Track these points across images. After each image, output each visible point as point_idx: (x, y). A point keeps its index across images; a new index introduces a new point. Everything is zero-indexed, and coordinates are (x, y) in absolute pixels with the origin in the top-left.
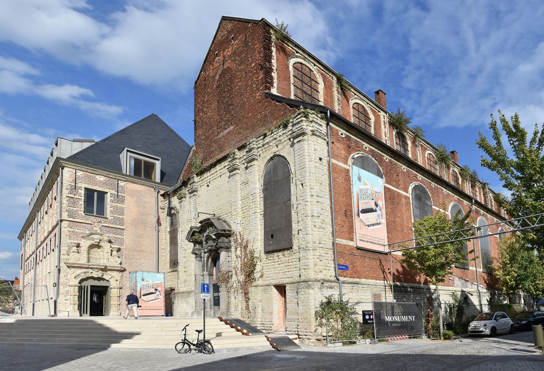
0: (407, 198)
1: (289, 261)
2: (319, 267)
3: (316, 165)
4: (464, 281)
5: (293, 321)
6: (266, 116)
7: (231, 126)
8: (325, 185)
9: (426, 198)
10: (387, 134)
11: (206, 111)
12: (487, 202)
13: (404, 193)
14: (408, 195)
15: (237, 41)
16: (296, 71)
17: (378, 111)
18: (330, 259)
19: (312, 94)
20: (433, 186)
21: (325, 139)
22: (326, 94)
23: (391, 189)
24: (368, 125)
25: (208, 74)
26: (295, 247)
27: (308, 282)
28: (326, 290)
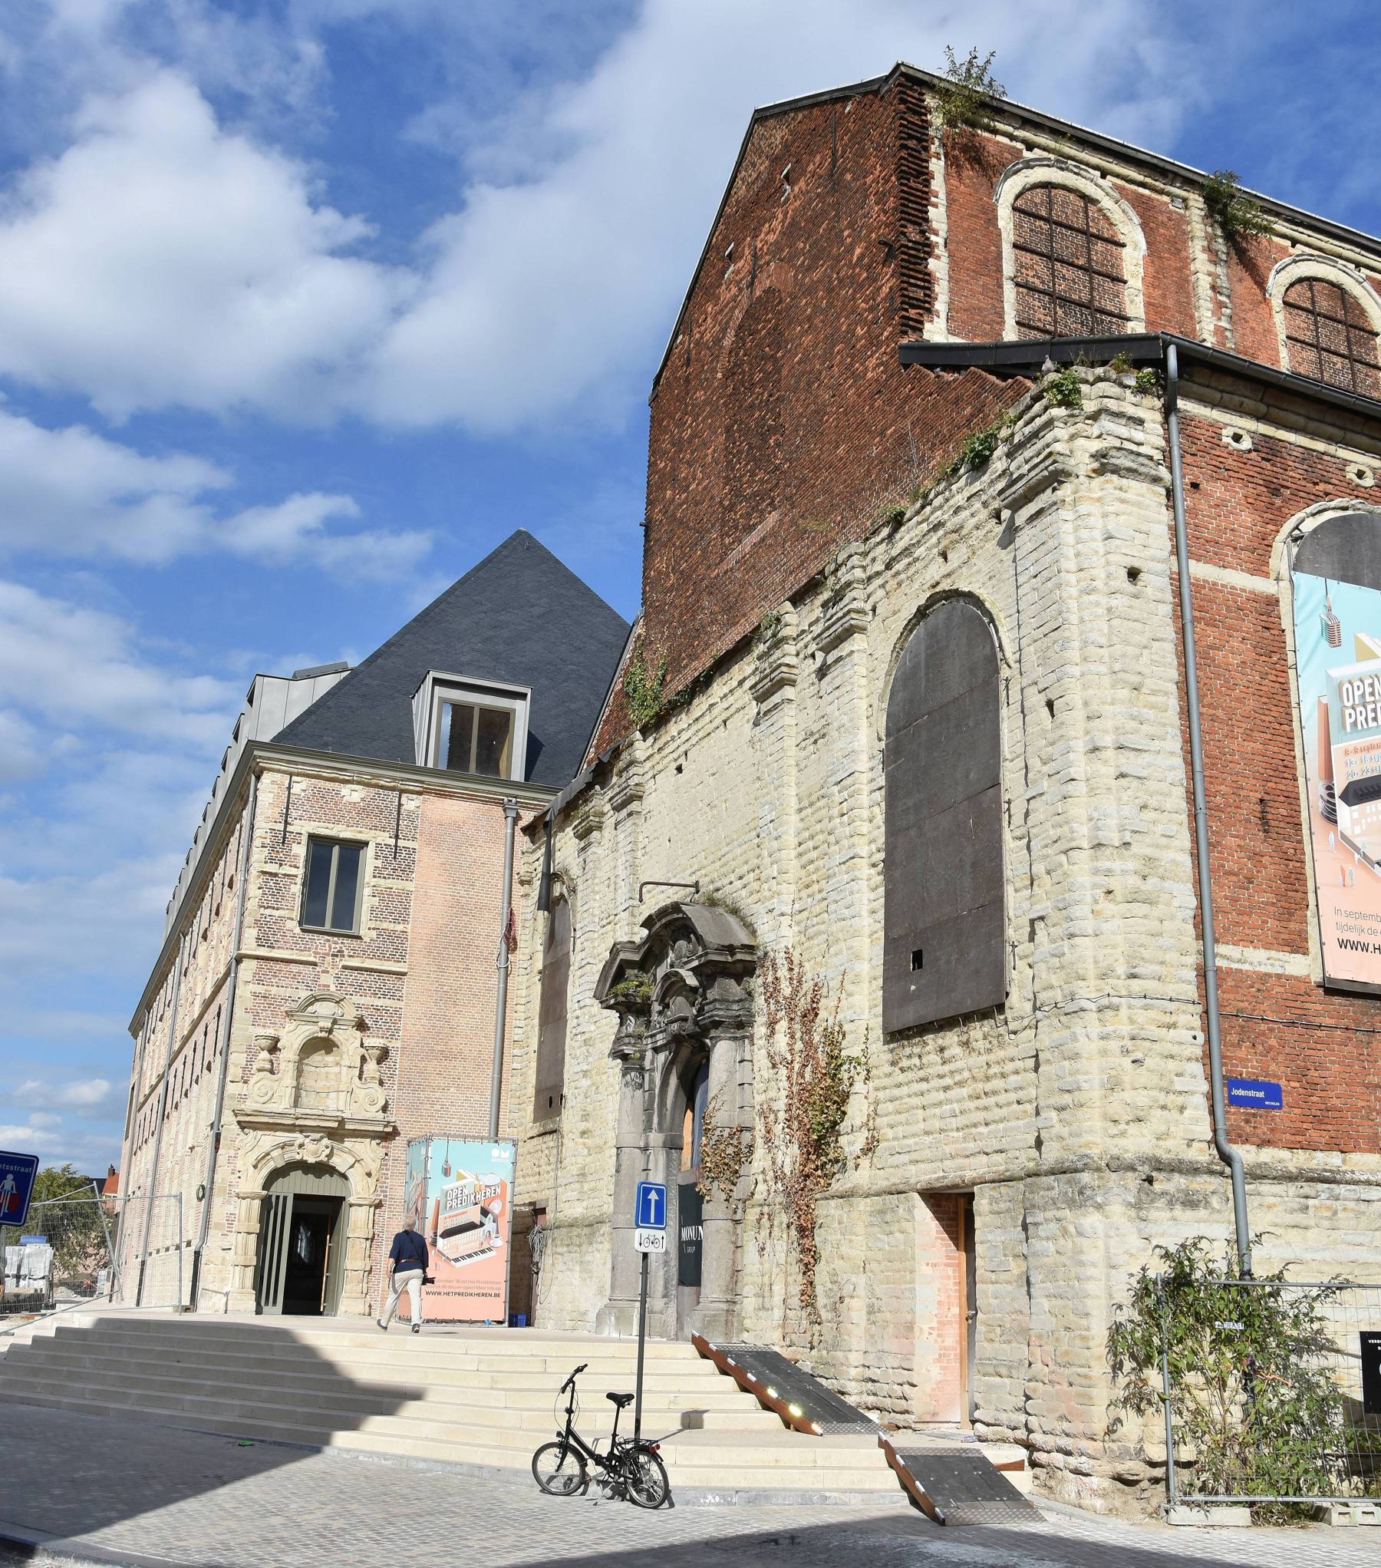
1: (991, 1072)
3: (1114, 603)
5: (1003, 1371)
6: (901, 440)
7: (770, 513)
8: (1154, 693)
11: (685, 479)
19: (1091, 301)
21: (1156, 480)
26: (1017, 1002)
27: (1076, 1171)
28: (1168, 1214)
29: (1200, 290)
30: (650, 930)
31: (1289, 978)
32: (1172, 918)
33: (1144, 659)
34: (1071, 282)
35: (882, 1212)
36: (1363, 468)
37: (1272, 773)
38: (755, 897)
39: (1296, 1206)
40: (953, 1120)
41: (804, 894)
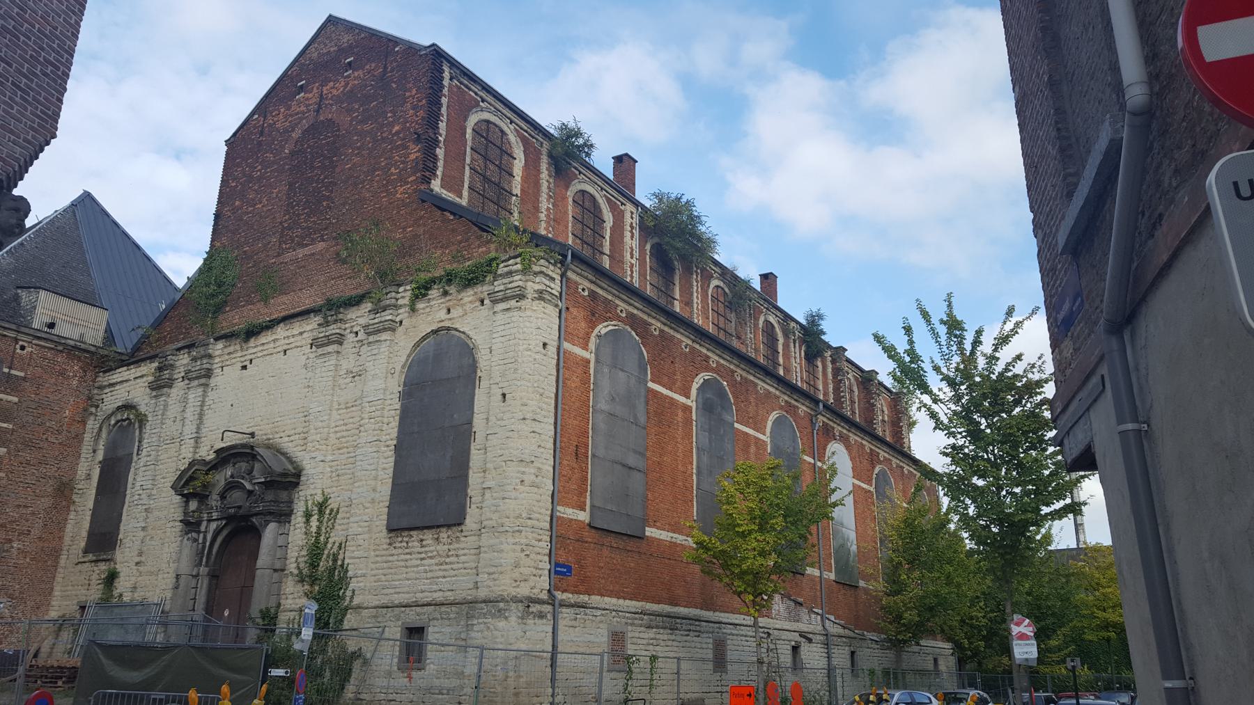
0: (687, 409)
1: (450, 553)
2: (522, 570)
3: (537, 357)
4: (792, 604)
5: (445, 692)
7: (319, 242)
8: (547, 397)
9: (723, 408)
12: (842, 394)
13: (682, 399)
14: (688, 402)
15: (360, 72)
18: (544, 552)
19: (500, 183)
20: (739, 379)
21: (557, 306)
22: (525, 179)
25: (271, 121)
26: (470, 522)
27: (497, 602)
28: (533, 622)
30: (1040, 660)
32: (545, 494)
33: (545, 383)
35: (375, 617)
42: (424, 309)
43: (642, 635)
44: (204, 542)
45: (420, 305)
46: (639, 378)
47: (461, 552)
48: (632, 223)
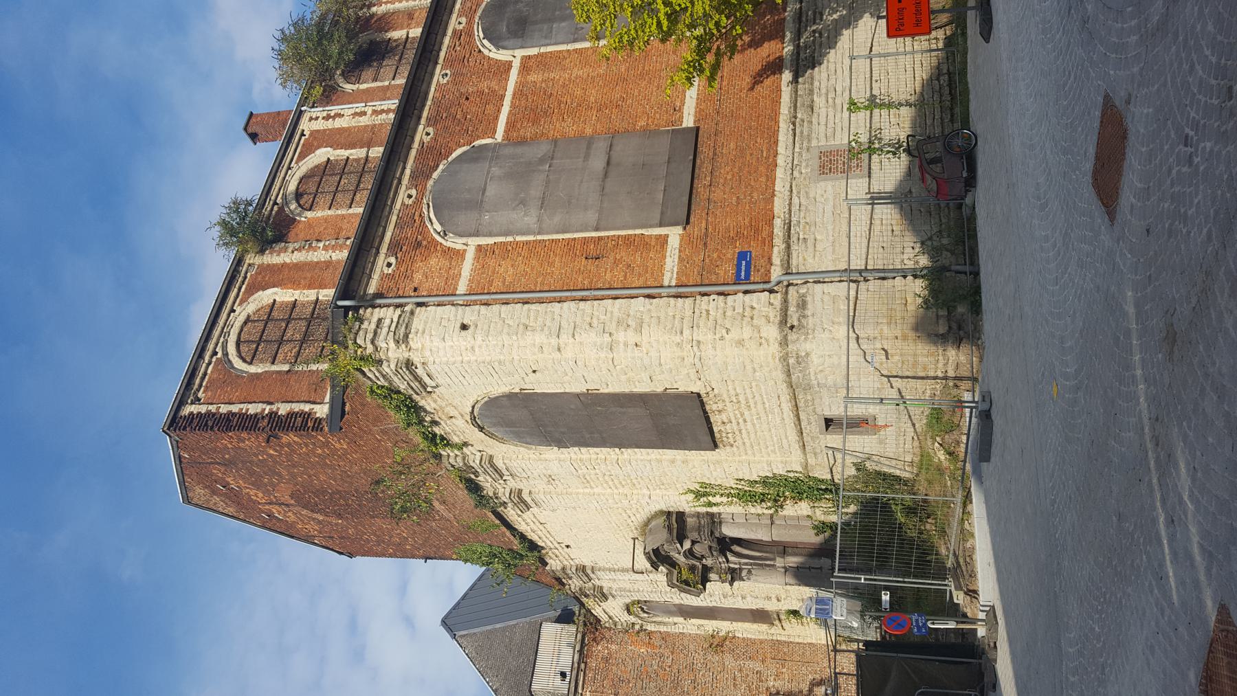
0: (526, 64)
8: (529, 317)
10: (358, 110)
11: (400, 538)
14: (516, 64)
16: (259, 356)
17: (303, 138)
18: (722, 305)
21: (412, 313)
22: (295, 284)
23: (508, 118)
24: (345, 165)
27: (788, 365)
28: (810, 318)
29: (302, 259)
31: (681, 246)
33: (511, 323)
34: (295, 331)
35: (815, 454)
36: (406, 195)
37: (571, 252)
38: (640, 510)
39: (804, 245)
40: (762, 419)
41: (638, 486)
42: (458, 436)
43: (823, 121)
44: (751, 564)
45: (456, 439)
46: (492, 159)
47: (732, 392)
48: (323, 118)
